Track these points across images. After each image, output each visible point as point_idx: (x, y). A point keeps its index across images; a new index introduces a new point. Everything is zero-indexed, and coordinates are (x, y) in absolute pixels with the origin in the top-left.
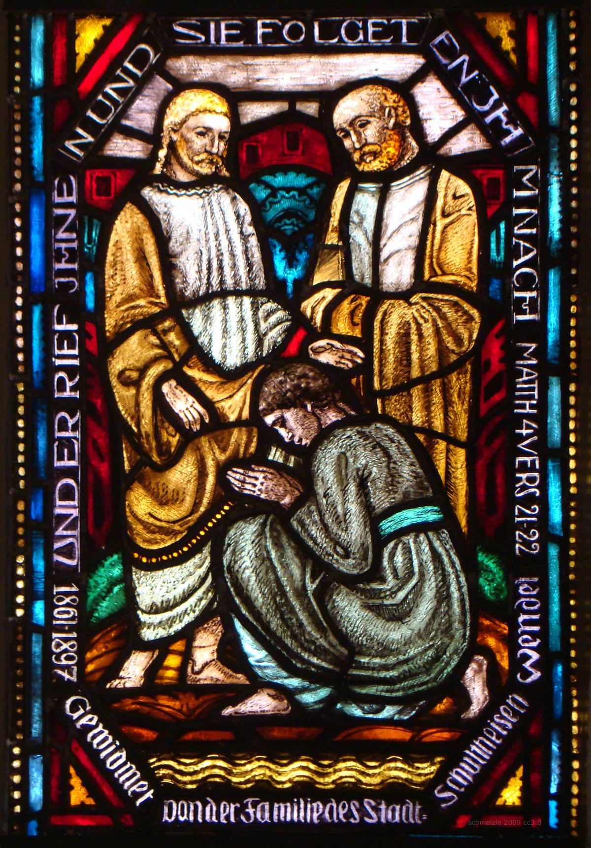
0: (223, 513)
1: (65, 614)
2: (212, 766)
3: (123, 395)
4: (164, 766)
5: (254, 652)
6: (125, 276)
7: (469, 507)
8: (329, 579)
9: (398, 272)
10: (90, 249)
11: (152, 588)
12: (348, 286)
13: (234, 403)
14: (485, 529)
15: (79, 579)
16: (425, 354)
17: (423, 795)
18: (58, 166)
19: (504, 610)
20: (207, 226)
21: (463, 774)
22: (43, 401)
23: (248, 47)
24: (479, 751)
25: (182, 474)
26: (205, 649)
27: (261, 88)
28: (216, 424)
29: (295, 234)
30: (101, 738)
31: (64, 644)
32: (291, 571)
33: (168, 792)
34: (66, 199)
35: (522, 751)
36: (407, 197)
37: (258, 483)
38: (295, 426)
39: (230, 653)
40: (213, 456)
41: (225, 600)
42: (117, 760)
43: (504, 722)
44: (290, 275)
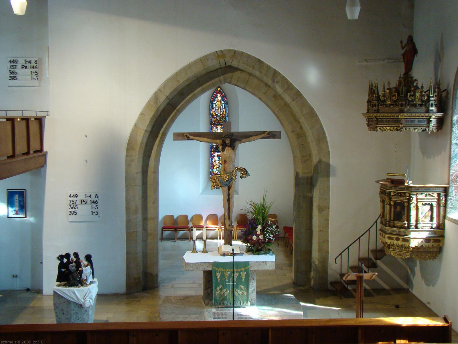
5: (218, 172)
7: (287, 296)
10: (257, 264)
20: (217, 159)
22: (211, 164)
23: (218, 153)
25: (216, 166)
27: (294, 278)
28: (217, 165)
31: (212, 172)
34: (212, 158)
37: (218, 167)
38: (219, 165)
39: (217, 172)
41: (217, 170)
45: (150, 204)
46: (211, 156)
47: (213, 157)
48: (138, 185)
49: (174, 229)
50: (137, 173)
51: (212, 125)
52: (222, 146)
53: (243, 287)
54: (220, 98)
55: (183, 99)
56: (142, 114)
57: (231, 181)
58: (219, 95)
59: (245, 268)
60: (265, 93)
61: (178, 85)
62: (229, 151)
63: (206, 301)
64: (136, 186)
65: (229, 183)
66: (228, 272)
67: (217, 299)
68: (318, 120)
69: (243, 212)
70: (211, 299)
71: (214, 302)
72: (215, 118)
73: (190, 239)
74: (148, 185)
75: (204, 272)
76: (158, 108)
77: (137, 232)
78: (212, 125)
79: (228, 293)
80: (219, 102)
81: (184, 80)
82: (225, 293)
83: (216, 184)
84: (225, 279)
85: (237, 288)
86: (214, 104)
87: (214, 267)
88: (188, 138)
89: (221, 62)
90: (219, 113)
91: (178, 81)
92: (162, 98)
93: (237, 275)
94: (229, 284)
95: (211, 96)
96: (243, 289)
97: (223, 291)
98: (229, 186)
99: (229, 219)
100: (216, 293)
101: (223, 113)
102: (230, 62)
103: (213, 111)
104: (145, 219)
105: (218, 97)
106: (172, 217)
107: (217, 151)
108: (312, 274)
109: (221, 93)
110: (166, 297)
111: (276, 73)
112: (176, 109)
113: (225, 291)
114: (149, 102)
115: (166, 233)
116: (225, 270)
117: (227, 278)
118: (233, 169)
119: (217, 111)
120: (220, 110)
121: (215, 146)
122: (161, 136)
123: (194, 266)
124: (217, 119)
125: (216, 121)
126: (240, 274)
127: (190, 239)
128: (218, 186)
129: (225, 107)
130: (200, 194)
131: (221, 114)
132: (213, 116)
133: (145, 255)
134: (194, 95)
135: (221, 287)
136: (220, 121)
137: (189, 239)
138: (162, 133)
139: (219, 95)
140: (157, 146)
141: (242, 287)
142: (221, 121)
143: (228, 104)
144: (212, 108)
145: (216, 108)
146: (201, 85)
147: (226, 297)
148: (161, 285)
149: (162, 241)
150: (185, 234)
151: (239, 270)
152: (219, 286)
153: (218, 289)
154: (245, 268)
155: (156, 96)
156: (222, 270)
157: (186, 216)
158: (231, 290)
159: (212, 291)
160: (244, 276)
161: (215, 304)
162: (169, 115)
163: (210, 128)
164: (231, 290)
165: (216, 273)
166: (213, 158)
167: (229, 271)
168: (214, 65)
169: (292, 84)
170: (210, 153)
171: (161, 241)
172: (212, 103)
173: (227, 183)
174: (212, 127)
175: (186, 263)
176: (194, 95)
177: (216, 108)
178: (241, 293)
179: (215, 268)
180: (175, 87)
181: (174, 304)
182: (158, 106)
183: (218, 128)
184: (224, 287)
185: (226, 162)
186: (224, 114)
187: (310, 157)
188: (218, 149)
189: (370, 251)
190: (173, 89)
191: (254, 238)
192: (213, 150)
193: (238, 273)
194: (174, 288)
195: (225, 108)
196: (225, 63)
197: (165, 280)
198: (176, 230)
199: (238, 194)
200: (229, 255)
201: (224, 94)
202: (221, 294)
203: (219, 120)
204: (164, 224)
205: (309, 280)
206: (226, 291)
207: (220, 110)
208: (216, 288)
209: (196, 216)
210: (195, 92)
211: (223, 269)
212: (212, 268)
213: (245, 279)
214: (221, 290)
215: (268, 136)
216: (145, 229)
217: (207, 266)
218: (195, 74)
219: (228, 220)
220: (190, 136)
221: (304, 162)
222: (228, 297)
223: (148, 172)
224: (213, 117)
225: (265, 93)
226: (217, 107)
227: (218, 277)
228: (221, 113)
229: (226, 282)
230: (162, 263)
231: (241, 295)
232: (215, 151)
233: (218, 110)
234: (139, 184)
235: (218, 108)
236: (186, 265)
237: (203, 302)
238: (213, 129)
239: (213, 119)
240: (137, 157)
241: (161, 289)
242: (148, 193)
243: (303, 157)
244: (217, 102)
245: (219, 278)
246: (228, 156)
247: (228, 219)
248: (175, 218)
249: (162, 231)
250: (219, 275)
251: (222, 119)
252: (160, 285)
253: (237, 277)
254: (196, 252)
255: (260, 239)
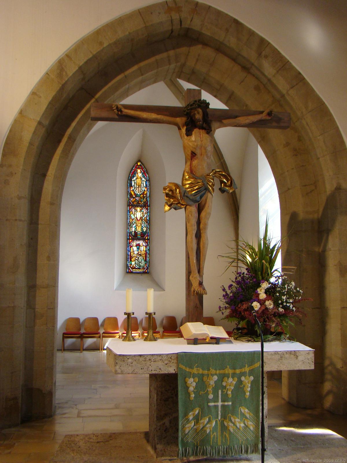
0: (114, 108)
1: (129, 264)
2: (135, 270)
3: (131, 255)
4: (133, 270)
5: (136, 265)
6: (132, 251)
8: (139, 262)
9: (142, 250)
10: (277, 357)
11: (132, 263)
12: (140, 251)
13: (136, 255)
14: (146, 260)
15: (130, 262)
16: (143, 254)
17: (143, 271)
18: (129, 246)
19: (146, 264)
20: (135, 248)
21: (145, 270)
22: (128, 255)
23: (136, 241)
24: (145, 269)
25: (134, 258)
26: (135, 265)
28: (135, 256)
29: (138, 249)
30: (130, 269)
31: (129, 265)
32: (138, 262)
33: (133, 271)
34: (129, 247)
35: (147, 269)
36: (143, 247)
37: (137, 259)
38: (138, 256)
39: (136, 265)
40: (135, 257)
41: (135, 263)
42: (131, 270)
43: (146, 268)
44: (138, 250)
45: (41, 261)
46: (128, 246)
47: (131, 247)
48: (20, 220)
49: (80, 335)
50: (20, 198)
51: (131, 207)
52: (186, 127)
53: (246, 410)
54: (140, 175)
55: (106, 83)
56: (34, 93)
57: (204, 194)
58: (139, 171)
59: (252, 367)
60: (242, 82)
61: (99, 50)
62: (201, 136)
63: (159, 447)
64: (16, 220)
65: (201, 197)
66: (212, 375)
67: (188, 441)
68: (332, 121)
69: (171, 314)
70: (174, 441)
71: (180, 448)
72: (134, 198)
73: (101, 350)
74: (40, 227)
75: (153, 377)
76: (63, 86)
77: (14, 307)
78: (131, 207)
79: (213, 425)
80: (139, 179)
81: (111, 42)
82: (207, 426)
83: (174, 201)
84: (207, 394)
85: (233, 415)
86: (133, 182)
87: (181, 366)
88: (120, 113)
89: (173, 18)
90: (139, 192)
91: (101, 43)
92: (71, 70)
93: (235, 383)
94: (216, 404)
95: (131, 168)
96: (248, 415)
97: (202, 421)
98: (198, 204)
99: (199, 272)
100: (187, 426)
101: (143, 194)
102: (189, 22)
103: (132, 189)
104: (32, 287)
105: (137, 173)
106: (78, 320)
107: (136, 239)
108: (327, 386)
109: (141, 168)
110: (66, 436)
111: (263, 42)
112: (93, 97)
113: (206, 422)
114: (47, 73)
115: (69, 341)
116: (206, 372)
117: (210, 389)
118: (209, 172)
119: (137, 189)
120: (140, 189)
121: (133, 233)
122: (67, 142)
123: (134, 363)
124: (136, 199)
125: (135, 201)
126: (240, 382)
127: (101, 350)
128: (177, 204)
129: (146, 185)
130: (115, 290)
131: (142, 194)
132: (131, 195)
133: (29, 355)
134: (126, 77)
135: (197, 412)
136: (140, 202)
137: (99, 350)
138: (68, 135)
139: (139, 171)
140: (58, 158)
141: (245, 410)
142: (141, 201)
143: (150, 182)
144: (131, 186)
145: (135, 186)
146: (137, 63)
147: (208, 435)
148: (58, 411)
149: (63, 352)
150: (95, 343)
151: (238, 371)
152: (192, 410)
153: (191, 418)
154: (252, 367)
155: (60, 65)
156: (201, 371)
157: (96, 320)
158: (219, 418)
159: (176, 420)
160: (250, 385)
161: (183, 453)
162: (83, 108)
163: (128, 210)
164: (219, 418)
165: (187, 379)
166: (131, 248)
167: (216, 374)
168: (161, 22)
169: (288, 61)
170: (127, 241)
171: (61, 352)
172: (131, 180)
173: (198, 197)
174: (130, 209)
175: (116, 355)
176: (126, 77)
177: (135, 186)
178: (242, 425)
179: (184, 368)
180: (95, 53)
181: (85, 454)
182: (64, 82)
183: (137, 210)
184: (205, 411)
185: (194, 156)
186: (145, 194)
187: (316, 186)
188: (137, 237)
189: (265, 376)
190: (91, 56)
191: (256, 305)
192: (130, 238)
193: (236, 379)
194: (83, 417)
195: (146, 187)
196: (181, 22)
197: (67, 403)
198: (82, 337)
199: (164, 290)
200: (207, 340)
201: (146, 169)
202: (196, 429)
203: (139, 201)
204: (66, 329)
205: (320, 398)
206: (209, 421)
207: (140, 189)
208: (186, 414)
209: (109, 319)
210: (127, 73)
211: (203, 369)
212: (178, 367)
213: (251, 391)
214: (197, 419)
215: (268, 118)
216: (30, 304)
217: (166, 362)
218: (130, 33)
219: (197, 274)
220: (123, 110)
221: (307, 194)
222: (212, 436)
223: (41, 202)
224: (131, 197)
225: (242, 82)
226: (137, 185)
227: (191, 389)
228: (141, 192)
229: (209, 401)
230: (59, 378)
231: (241, 429)
232: (133, 240)
233: (138, 189)
234: (23, 219)
235: (137, 186)
236: (117, 361)
237: (149, 448)
238: (131, 211)
239: (132, 199)
240: (21, 167)
241: (58, 418)
242: (39, 240)
243: (305, 186)
244: (136, 179)
245: (193, 391)
246: (199, 143)
247: (197, 271)
248: (81, 321)
249: (64, 337)
250: (192, 383)
251: (142, 200)
252: (57, 413)
253: (232, 388)
254: (132, 339)
255: (267, 309)
